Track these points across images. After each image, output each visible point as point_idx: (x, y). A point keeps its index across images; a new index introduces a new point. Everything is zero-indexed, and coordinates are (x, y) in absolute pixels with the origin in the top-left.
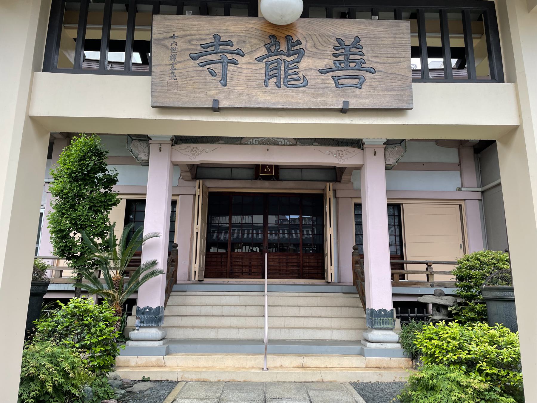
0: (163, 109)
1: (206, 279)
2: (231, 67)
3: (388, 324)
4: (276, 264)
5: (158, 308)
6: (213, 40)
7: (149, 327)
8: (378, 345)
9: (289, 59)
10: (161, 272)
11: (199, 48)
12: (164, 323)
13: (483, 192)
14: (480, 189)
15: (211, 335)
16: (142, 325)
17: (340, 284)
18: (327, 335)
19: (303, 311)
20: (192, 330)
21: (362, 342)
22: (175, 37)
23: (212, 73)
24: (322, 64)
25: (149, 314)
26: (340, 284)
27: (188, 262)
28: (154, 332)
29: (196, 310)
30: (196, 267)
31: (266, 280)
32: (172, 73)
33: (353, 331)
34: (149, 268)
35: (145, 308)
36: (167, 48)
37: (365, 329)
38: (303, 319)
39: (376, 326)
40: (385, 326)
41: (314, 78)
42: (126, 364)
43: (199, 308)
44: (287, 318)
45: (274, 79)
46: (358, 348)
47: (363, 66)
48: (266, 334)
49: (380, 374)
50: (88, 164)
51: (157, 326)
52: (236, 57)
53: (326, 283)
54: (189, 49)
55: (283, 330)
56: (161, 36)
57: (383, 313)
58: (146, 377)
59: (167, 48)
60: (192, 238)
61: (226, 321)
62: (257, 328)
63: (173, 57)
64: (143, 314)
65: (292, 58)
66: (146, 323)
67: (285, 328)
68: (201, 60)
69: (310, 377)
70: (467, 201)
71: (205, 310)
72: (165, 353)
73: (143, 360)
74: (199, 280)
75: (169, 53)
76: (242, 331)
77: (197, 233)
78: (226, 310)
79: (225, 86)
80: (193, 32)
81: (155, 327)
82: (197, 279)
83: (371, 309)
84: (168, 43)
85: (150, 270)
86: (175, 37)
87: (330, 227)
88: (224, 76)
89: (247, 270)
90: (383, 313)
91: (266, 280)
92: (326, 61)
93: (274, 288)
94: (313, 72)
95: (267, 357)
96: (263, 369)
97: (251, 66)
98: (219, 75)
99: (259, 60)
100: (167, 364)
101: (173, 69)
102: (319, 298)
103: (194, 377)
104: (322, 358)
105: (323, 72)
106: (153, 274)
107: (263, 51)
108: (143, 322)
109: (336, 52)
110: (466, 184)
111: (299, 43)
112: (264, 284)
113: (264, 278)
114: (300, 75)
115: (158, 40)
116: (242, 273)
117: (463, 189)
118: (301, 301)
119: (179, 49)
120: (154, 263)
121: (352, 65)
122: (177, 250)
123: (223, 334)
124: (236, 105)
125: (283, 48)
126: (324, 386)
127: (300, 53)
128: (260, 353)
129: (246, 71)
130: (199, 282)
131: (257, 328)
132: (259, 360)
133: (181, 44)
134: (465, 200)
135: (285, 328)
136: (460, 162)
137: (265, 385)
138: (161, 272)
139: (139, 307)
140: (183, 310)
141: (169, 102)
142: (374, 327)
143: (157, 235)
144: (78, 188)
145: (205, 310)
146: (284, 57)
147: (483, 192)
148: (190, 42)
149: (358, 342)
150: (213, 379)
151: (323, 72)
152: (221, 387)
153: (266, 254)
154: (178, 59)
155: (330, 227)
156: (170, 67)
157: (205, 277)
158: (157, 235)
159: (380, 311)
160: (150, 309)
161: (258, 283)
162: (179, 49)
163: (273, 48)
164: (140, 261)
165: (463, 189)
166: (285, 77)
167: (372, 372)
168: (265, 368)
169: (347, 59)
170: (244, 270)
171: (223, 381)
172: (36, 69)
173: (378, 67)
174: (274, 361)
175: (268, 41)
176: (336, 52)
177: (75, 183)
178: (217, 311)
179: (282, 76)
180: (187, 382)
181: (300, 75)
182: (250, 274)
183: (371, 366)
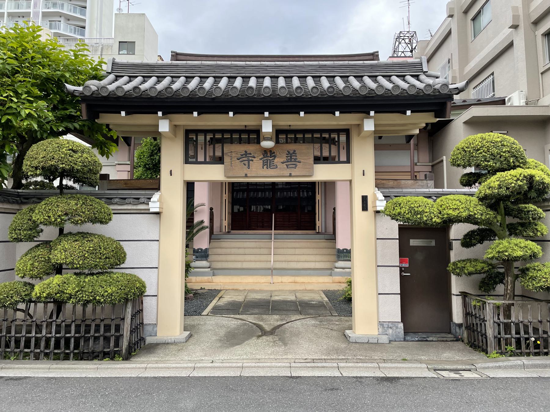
0: (228, 177)
1: (232, 231)
2: (251, 162)
3: (348, 258)
4: (281, 220)
5: (206, 249)
6: (245, 153)
7: (201, 260)
8: (341, 270)
9: (271, 159)
10: (207, 227)
11: (240, 156)
12: (211, 258)
13: (432, 166)
14: (431, 164)
15: (238, 265)
16: (197, 259)
17: (326, 233)
18: (312, 265)
19: (298, 251)
20: (226, 262)
21: (333, 269)
22: (231, 152)
23: (245, 165)
24: (282, 160)
25: (201, 252)
26: (326, 233)
27: (219, 219)
28: (204, 263)
29: (228, 251)
30: (225, 223)
31: (273, 231)
32: (231, 165)
33: (329, 262)
34: (199, 225)
35: (198, 249)
36: (229, 156)
37: (336, 262)
38: (297, 256)
39: (341, 259)
40: (346, 259)
41: (280, 165)
42: (190, 281)
43: (230, 249)
44: (286, 255)
45: (266, 166)
46: (329, 271)
47: (297, 160)
48: (272, 265)
49: (340, 285)
50: (156, 158)
51: (206, 260)
52: (253, 158)
53: (316, 233)
54: (236, 156)
55: (284, 262)
56: (227, 152)
57: (345, 251)
58: (203, 288)
59: (229, 156)
60: (221, 203)
61: (248, 258)
62: (267, 261)
63: (231, 159)
64: (197, 252)
65: (272, 158)
66: (200, 258)
67: (285, 261)
68: (241, 160)
69: (298, 287)
70: (420, 172)
71: (233, 251)
72: (212, 275)
73: (199, 279)
74: (228, 232)
75: (230, 158)
76: (258, 263)
77: (225, 200)
78: (247, 251)
79: (249, 168)
80: (237, 150)
81: (205, 260)
82: (227, 231)
83: (338, 249)
84: (229, 154)
85: (201, 226)
86: (231, 152)
87: (319, 194)
88: (249, 166)
89: (261, 225)
90: (345, 251)
91: (273, 231)
92: (284, 159)
93: (279, 236)
94: (279, 163)
95: (273, 277)
96: (271, 283)
97: (258, 162)
98: (247, 165)
99: (261, 159)
100: (214, 281)
101: (231, 163)
102: (309, 243)
103: (231, 288)
104: (306, 277)
105: (283, 163)
106: (203, 228)
107: (262, 156)
108: (198, 257)
109: (287, 156)
110: (421, 160)
111: (274, 153)
112: (272, 234)
113: (272, 230)
114: (275, 164)
115: (226, 153)
116: (257, 226)
117: (418, 164)
118: (297, 245)
119: (233, 156)
120: (202, 222)
121: (293, 160)
122: (213, 212)
123: (246, 265)
124: (253, 175)
125: (269, 155)
126: (306, 291)
127: (275, 157)
128: (269, 275)
129: (256, 163)
130: (227, 233)
131: (267, 261)
132: (269, 279)
133: (234, 155)
134: (419, 172)
135: (285, 261)
136: (418, 144)
137: (271, 291)
138: (207, 227)
139: (194, 249)
140: (219, 251)
141: (230, 175)
142: (339, 259)
143: (203, 205)
144: (151, 175)
145: (233, 251)
146: (269, 158)
147: (432, 166)
148: (237, 154)
149: (331, 269)
150: (241, 288)
151: (283, 163)
152: (247, 292)
153: (273, 214)
154: (233, 160)
155: (319, 194)
156: (230, 163)
157: (232, 230)
158: (203, 205)
159: (343, 250)
160: (201, 249)
161: (286, 233)
162: (233, 156)
163: (265, 155)
164: (193, 219)
165: (418, 164)
166: (270, 165)
167: (335, 284)
168: (272, 283)
169: (291, 158)
170: (258, 225)
171: (247, 290)
172: (184, 164)
173: (302, 161)
174: (277, 279)
175: (264, 152)
176: (287, 156)
177: (149, 171)
178: (241, 251)
179: (269, 165)
180: (226, 290)
181: (275, 164)
182: (263, 228)
183: (335, 282)
